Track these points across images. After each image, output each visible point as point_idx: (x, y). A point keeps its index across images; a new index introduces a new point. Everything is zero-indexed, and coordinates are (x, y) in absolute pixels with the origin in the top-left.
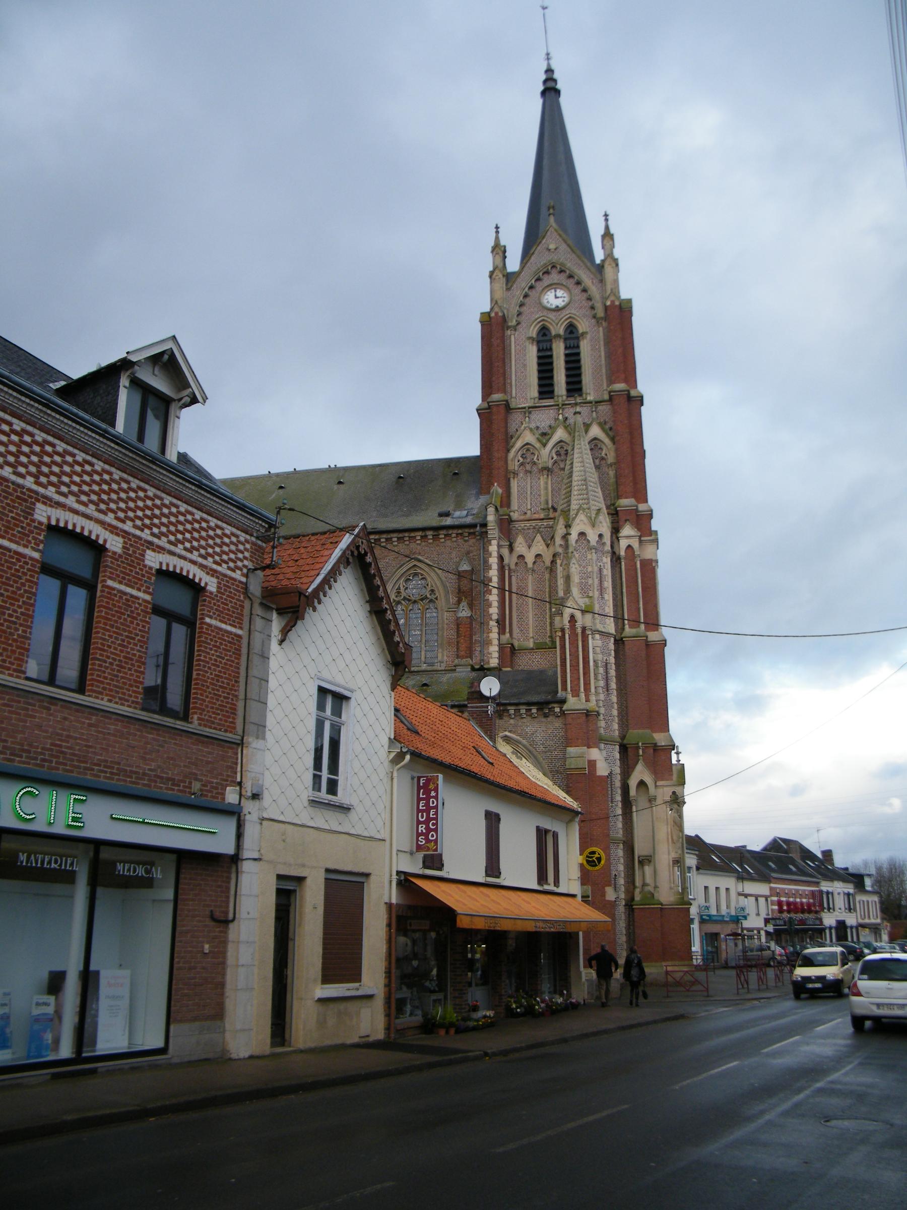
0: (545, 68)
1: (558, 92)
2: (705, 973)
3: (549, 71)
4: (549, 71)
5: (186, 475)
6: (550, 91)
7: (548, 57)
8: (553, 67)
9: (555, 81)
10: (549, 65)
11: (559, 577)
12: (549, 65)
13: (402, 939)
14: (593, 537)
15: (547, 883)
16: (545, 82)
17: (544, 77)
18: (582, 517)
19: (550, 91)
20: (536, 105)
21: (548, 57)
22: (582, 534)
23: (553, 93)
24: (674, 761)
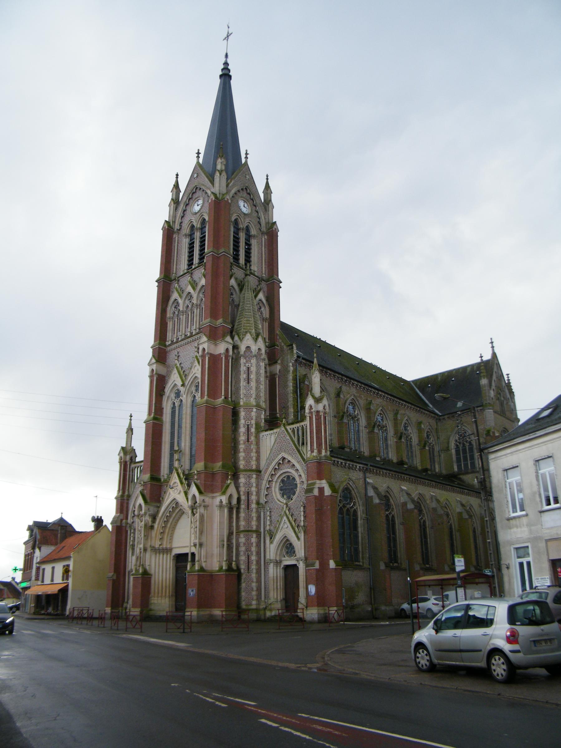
0: (223, 62)
1: (230, 77)
2: (165, 624)
3: (226, 64)
4: (226, 64)
5: (179, 437)
6: (226, 76)
7: (227, 56)
8: (229, 62)
9: (229, 71)
10: (226, 60)
11: (242, 373)
12: (226, 60)
13: (514, 417)
14: (254, 348)
15: (517, 512)
16: (222, 70)
17: (222, 67)
18: (248, 336)
19: (226, 76)
20: (217, 82)
21: (227, 56)
22: (248, 348)
23: (227, 77)
24: (316, 670)
